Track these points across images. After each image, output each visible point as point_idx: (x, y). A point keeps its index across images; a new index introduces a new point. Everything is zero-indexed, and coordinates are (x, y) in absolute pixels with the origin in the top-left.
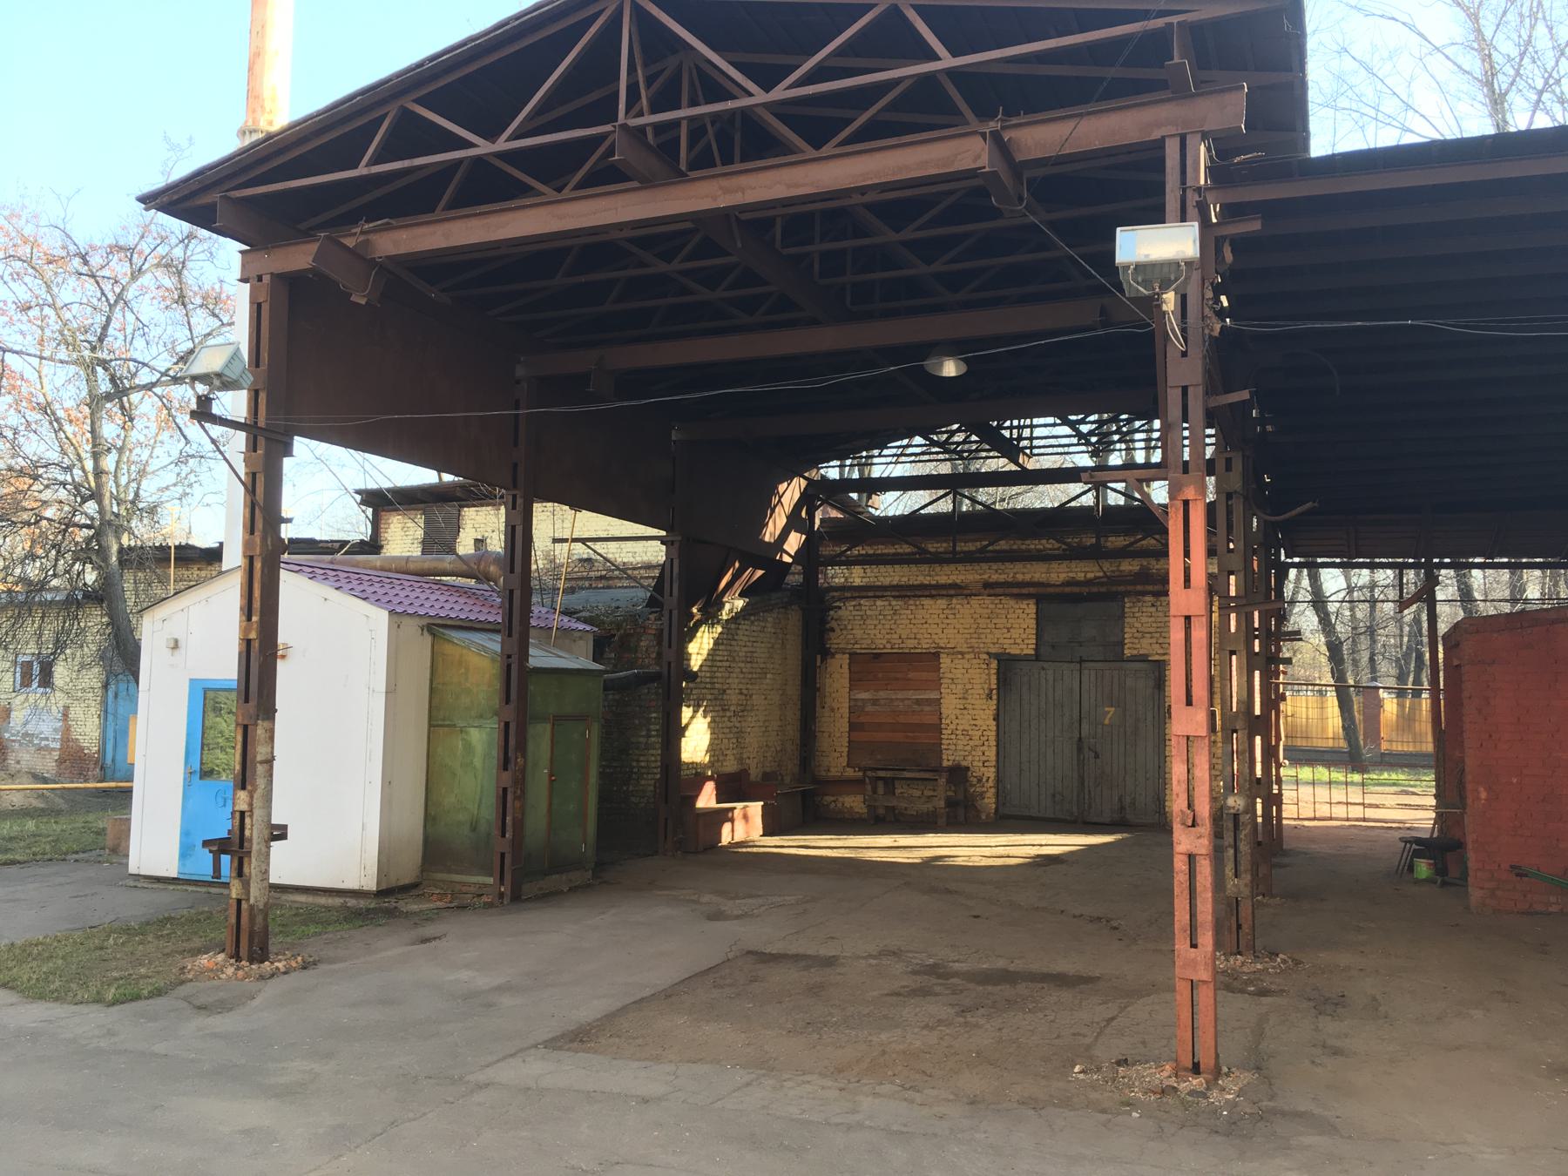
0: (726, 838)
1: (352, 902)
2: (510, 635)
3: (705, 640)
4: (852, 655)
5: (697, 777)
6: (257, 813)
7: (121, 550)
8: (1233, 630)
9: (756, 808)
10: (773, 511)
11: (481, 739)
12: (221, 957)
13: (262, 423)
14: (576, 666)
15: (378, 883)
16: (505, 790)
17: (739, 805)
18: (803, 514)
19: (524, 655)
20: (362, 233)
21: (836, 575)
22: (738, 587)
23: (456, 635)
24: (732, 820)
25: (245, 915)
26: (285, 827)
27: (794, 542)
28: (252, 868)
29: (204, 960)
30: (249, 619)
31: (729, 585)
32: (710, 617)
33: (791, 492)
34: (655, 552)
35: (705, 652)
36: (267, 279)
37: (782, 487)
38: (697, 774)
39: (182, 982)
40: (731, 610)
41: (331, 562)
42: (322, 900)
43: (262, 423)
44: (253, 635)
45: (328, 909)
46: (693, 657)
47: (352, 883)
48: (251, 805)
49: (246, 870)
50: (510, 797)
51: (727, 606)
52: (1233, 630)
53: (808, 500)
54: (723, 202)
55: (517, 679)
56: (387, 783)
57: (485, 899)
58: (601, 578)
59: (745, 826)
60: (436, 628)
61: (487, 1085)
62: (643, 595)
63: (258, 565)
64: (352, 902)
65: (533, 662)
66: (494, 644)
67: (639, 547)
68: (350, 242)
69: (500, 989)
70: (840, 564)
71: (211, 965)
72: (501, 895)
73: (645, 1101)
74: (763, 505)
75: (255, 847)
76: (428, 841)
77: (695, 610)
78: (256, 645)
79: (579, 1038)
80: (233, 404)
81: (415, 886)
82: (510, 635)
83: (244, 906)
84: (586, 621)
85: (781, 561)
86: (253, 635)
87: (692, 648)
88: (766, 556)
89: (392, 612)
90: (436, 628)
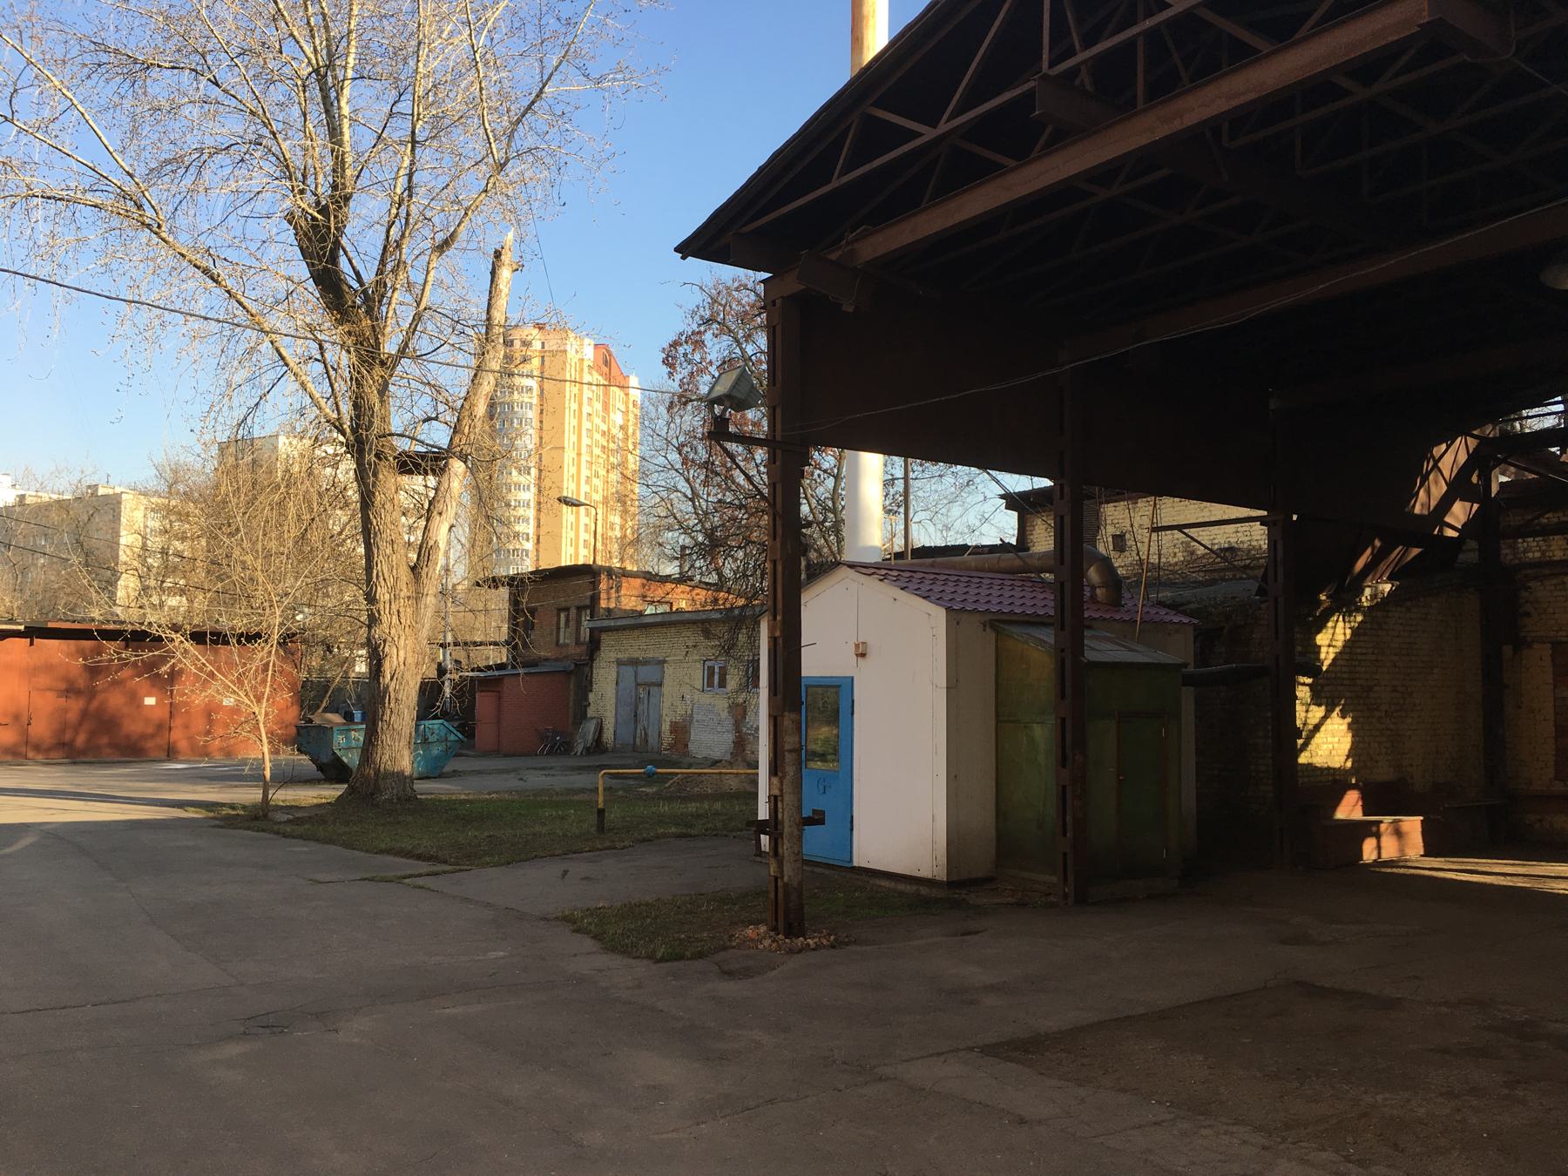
0: (1369, 851)
1: (924, 891)
2: (1063, 628)
3: (1339, 630)
4: (1557, 645)
5: (1332, 784)
6: (787, 798)
7: (808, 566)
9: (1413, 825)
10: (1425, 478)
11: (1042, 734)
12: (763, 929)
13: (778, 438)
14: (1146, 660)
15: (948, 874)
16: (1064, 787)
17: (1388, 819)
18: (1474, 479)
19: (1078, 647)
20: (848, 244)
21: (1532, 549)
22: (1385, 567)
23: (1015, 630)
24: (1378, 836)
25: (781, 895)
27: (1459, 513)
28: (786, 848)
29: (750, 932)
31: (1369, 568)
32: (1345, 603)
33: (1452, 456)
34: (1255, 536)
35: (1340, 644)
36: (779, 302)
37: (1438, 450)
38: (1335, 781)
39: (725, 948)
40: (1374, 596)
41: (932, 566)
42: (901, 887)
44: (778, 634)
45: (901, 894)
46: (1324, 650)
47: (925, 873)
48: (781, 790)
50: (1069, 796)
51: (1368, 591)
53: (1481, 461)
54: (1162, 131)
55: (1075, 676)
56: (952, 778)
57: (1052, 899)
58: (1246, 567)
59: (1400, 842)
60: (998, 624)
61: (887, 1079)
62: (1253, 586)
64: (924, 891)
65: (1090, 656)
66: (1048, 636)
67: (1238, 529)
68: (833, 256)
69: (992, 988)
70: (1534, 534)
71: (754, 936)
72: (1066, 896)
73: (1022, 1121)
74: (1414, 470)
75: (787, 830)
76: (1000, 836)
77: (1323, 597)
78: (780, 641)
79: (1024, 1049)
80: (755, 418)
81: (990, 880)
82: (1063, 628)
83: (780, 883)
84: (1191, 614)
85: (1441, 536)
86: (778, 634)
87: (1322, 639)
88: (1425, 529)
89: (949, 609)
90: (998, 624)
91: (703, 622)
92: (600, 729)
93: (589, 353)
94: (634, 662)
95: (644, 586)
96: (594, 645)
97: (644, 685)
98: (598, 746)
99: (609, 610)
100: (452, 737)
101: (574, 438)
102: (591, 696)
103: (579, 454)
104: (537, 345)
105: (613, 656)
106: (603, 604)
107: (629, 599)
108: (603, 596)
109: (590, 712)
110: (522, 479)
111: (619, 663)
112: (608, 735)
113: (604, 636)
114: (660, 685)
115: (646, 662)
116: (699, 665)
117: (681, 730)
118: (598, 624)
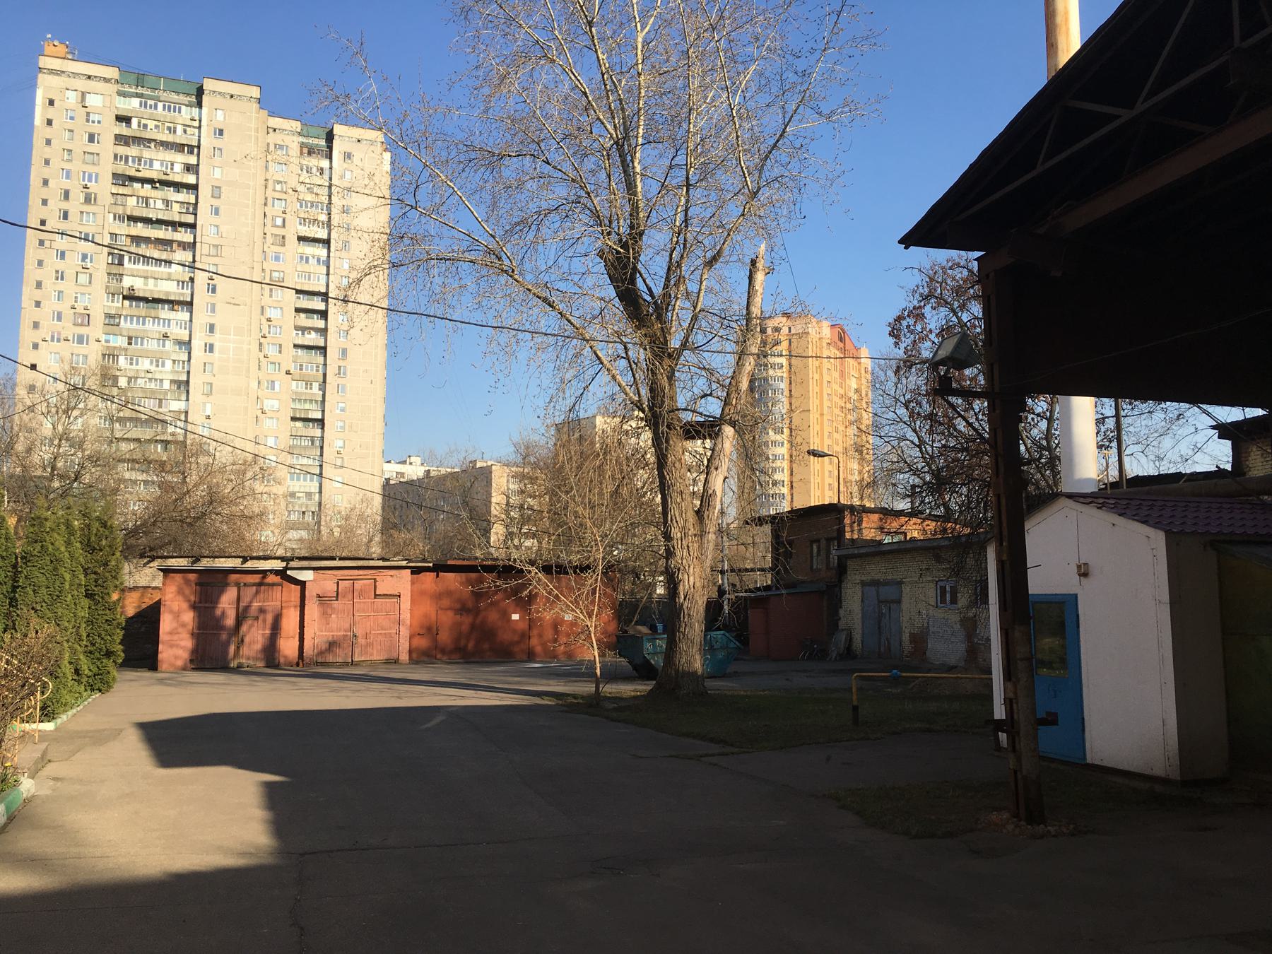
8: (1259, 412)
12: (1005, 815)
13: (997, 390)
26: (1056, 714)
29: (994, 816)
30: (1001, 544)
43: (997, 390)
44: (1005, 558)
47: (1159, 771)
48: (1015, 693)
49: (1017, 747)
52: (1259, 412)
63: (1003, 501)
83: (1019, 776)
86: (1005, 558)
91: (933, 548)
92: (850, 639)
93: (826, 332)
94: (876, 583)
95: (881, 520)
96: (842, 570)
97: (885, 602)
98: (849, 653)
99: (852, 540)
100: (732, 645)
101: (817, 402)
102: (841, 612)
103: (822, 415)
104: (785, 330)
105: (858, 578)
106: (848, 535)
107: (869, 530)
108: (847, 529)
109: (842, 625)
110: (778, 438)
111: (863, 584)
112: (857, 643)
113: (849, 562)
114: (899, 602)
115: (887, 583)
116: (933, 585)
117: (919, 640)
118: (844, 552)
